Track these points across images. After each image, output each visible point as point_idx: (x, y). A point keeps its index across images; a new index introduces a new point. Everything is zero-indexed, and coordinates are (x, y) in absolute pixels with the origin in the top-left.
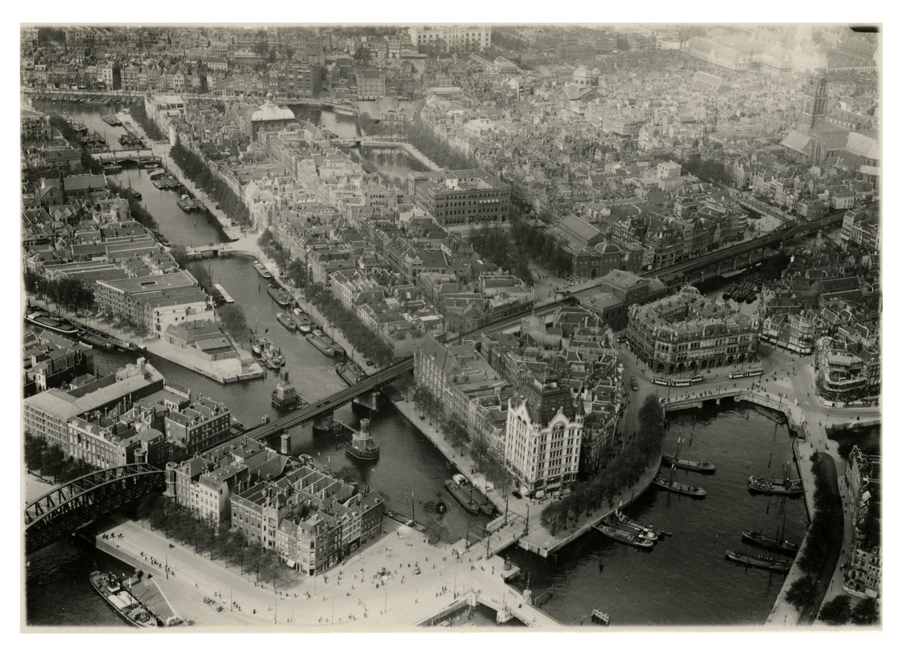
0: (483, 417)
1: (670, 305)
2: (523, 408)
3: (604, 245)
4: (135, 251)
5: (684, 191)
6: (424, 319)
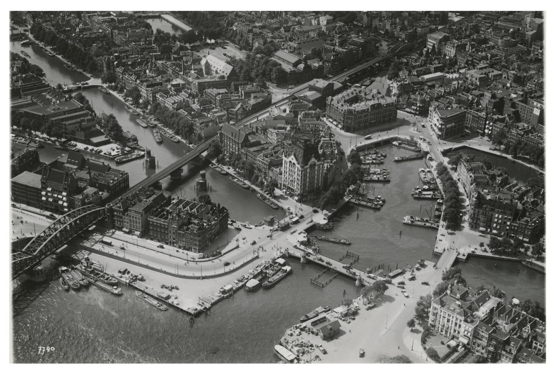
0: (267, 163)
1: (348, 95)
2: (293, 157)
3: (301, 66)
4: (39, 91)
5: (338, 32)
6: (216, 115)
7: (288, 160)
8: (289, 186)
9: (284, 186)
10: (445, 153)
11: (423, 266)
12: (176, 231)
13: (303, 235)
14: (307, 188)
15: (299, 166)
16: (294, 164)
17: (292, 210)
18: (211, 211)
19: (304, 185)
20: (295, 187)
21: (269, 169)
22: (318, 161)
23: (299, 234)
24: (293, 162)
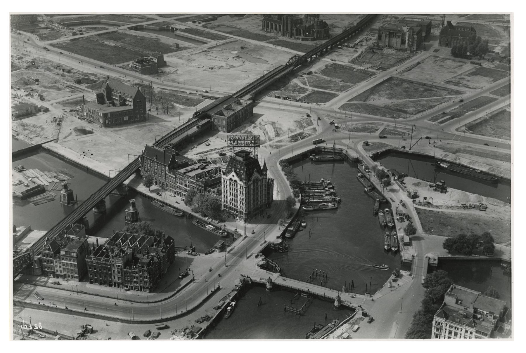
2: (233, 173)
7: (228, 178)
8: (231, 206)
9: (224, 207)
11: (399, 276)
12: (121, 269)
13: (260, 258)
14: (252, 206)
15: (242, 183)
16: (236, 181)
17: (241, 232)
18: (155, 242)
19: (248, 203)
20: (239, 207)
21: (205, 190)
22: (261, 176)
23: (257, 257)
24: (234, 179)
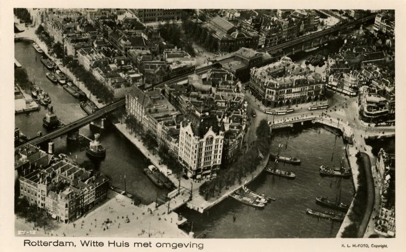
0: (166, 132)
1: (275, 68)
3: (237, 33)
6: (132, 76)
10: (369, 141)
